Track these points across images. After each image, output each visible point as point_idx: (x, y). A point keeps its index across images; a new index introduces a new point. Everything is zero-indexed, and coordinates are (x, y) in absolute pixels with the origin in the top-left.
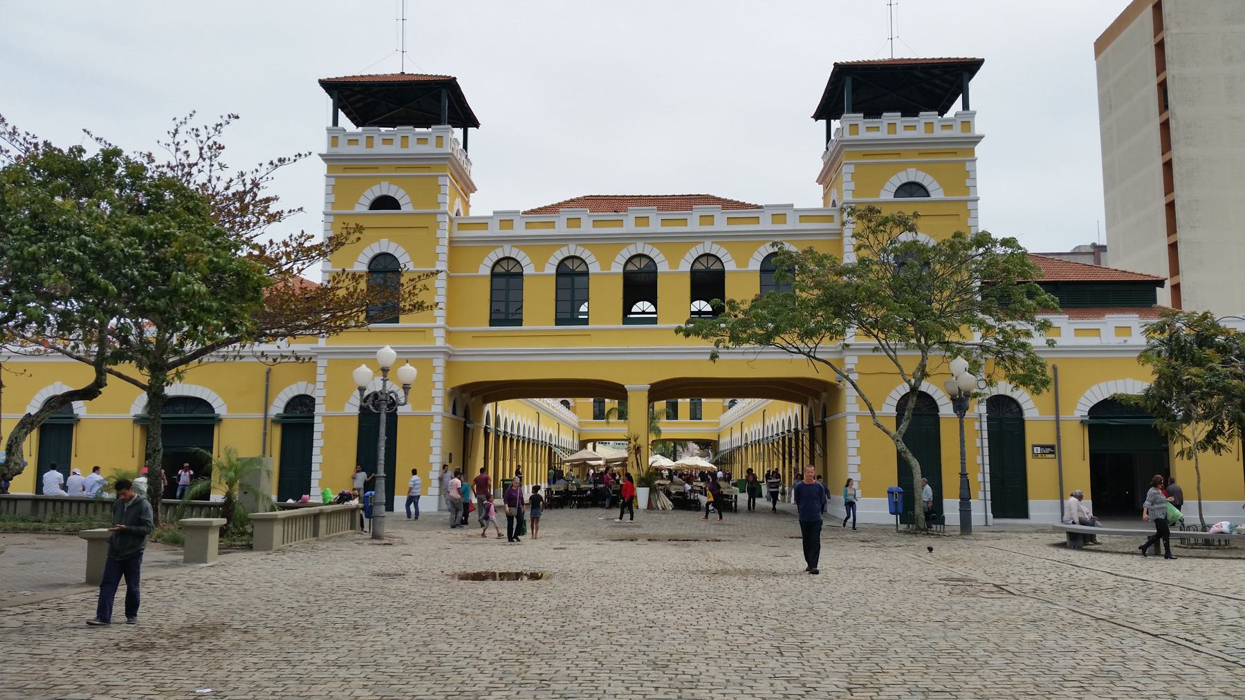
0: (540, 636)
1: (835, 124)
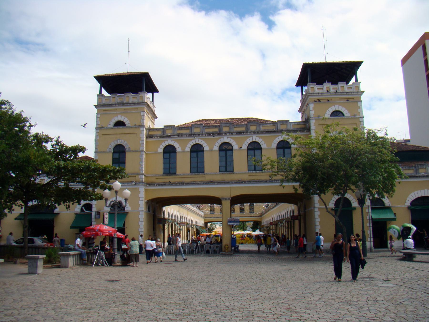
0: (170, 316)
1: (305, 88)
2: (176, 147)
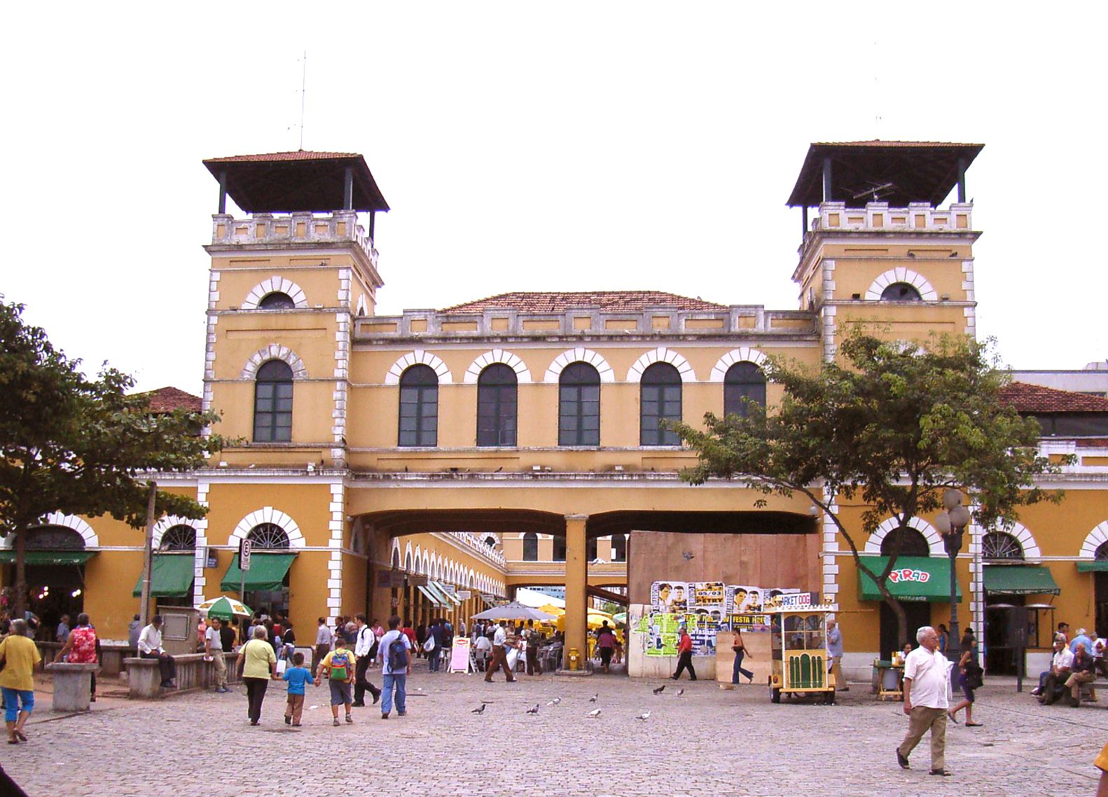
1: (813, 212)
2: (438, 372)
